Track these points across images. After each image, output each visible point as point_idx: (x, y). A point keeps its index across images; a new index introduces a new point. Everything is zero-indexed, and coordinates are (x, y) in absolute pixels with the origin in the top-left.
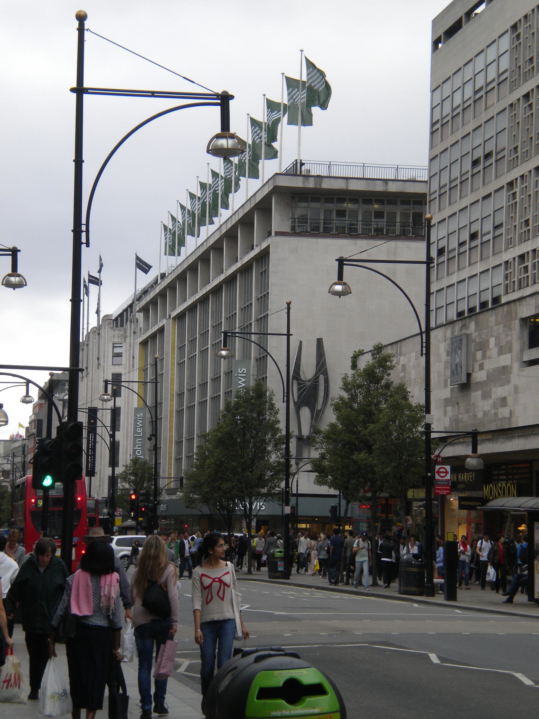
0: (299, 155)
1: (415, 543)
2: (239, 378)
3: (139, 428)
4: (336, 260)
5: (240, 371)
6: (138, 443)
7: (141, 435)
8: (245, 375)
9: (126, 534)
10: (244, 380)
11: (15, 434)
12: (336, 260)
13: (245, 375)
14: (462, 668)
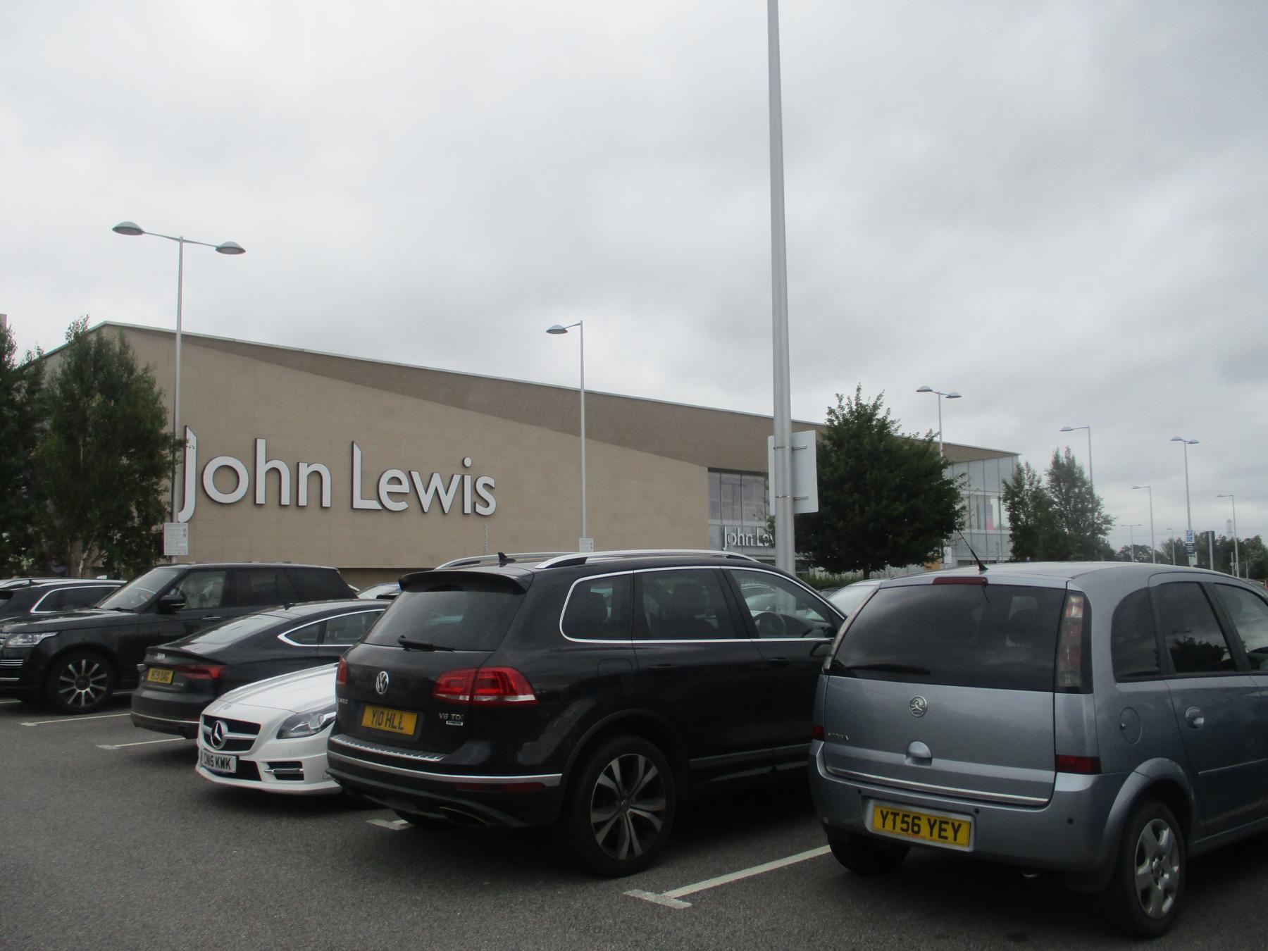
0: (1190, 527)
1: (118, 570)
2: (457, 479)
3: (405, 488)
4: (829, 408)
5: (486, 486)
6: (304, 471)
8: (468, 509)
9: (119, 579)
10: (447, 501)
11: (1105, 512)
12: (829, 408)
13: (468, 509)
14: (951, 786)
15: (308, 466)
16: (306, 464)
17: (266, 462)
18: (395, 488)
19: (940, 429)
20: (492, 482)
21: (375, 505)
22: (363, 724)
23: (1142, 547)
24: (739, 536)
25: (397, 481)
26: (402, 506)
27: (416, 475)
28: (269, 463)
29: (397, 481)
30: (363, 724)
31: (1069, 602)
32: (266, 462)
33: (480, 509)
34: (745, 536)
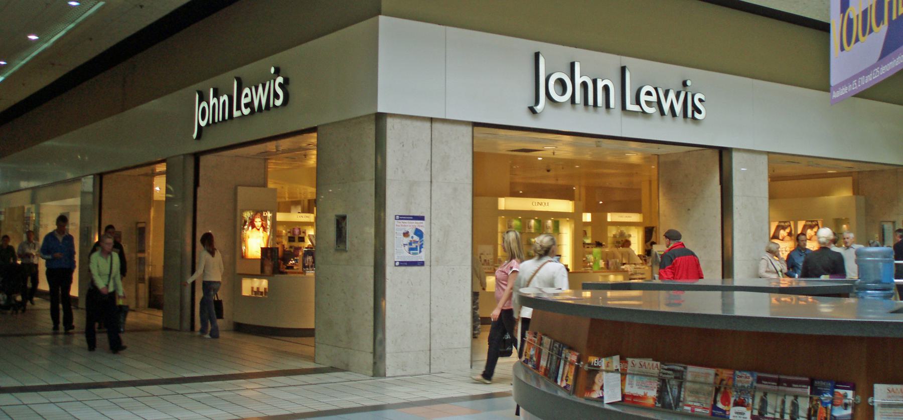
5: (701, 100)
6: (600, 84)
7: (630, 106)
10: (678, 108)
15: (602, 80)
16: (601, 80)
17: (581, 77)
18: (649, 98)
19: (890, 222)
20: (703, 98)
21: (636, 108)
22: (590, 221)
23: (856, 263)
24: (578, 80)
25: (649, 93)
28: (604, 81)
30: (590, 221)
31: (155, 191)
32: (581, 77)
34: (595, 82)
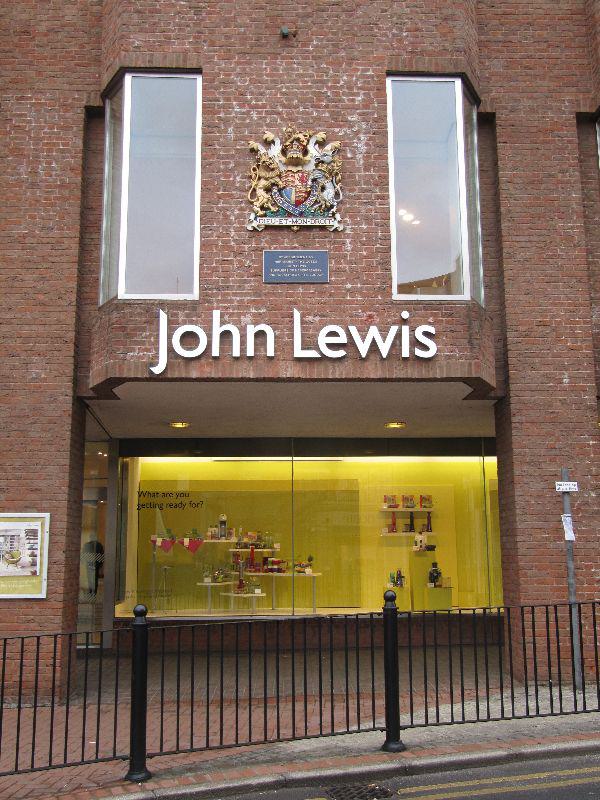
6: (251, 330)
8: (406, 353)
10: (385, 348)
25: (333, 334)
26: (341, 353)
27: (353, 330)
29: (333, 334)
33: (419, 353)
